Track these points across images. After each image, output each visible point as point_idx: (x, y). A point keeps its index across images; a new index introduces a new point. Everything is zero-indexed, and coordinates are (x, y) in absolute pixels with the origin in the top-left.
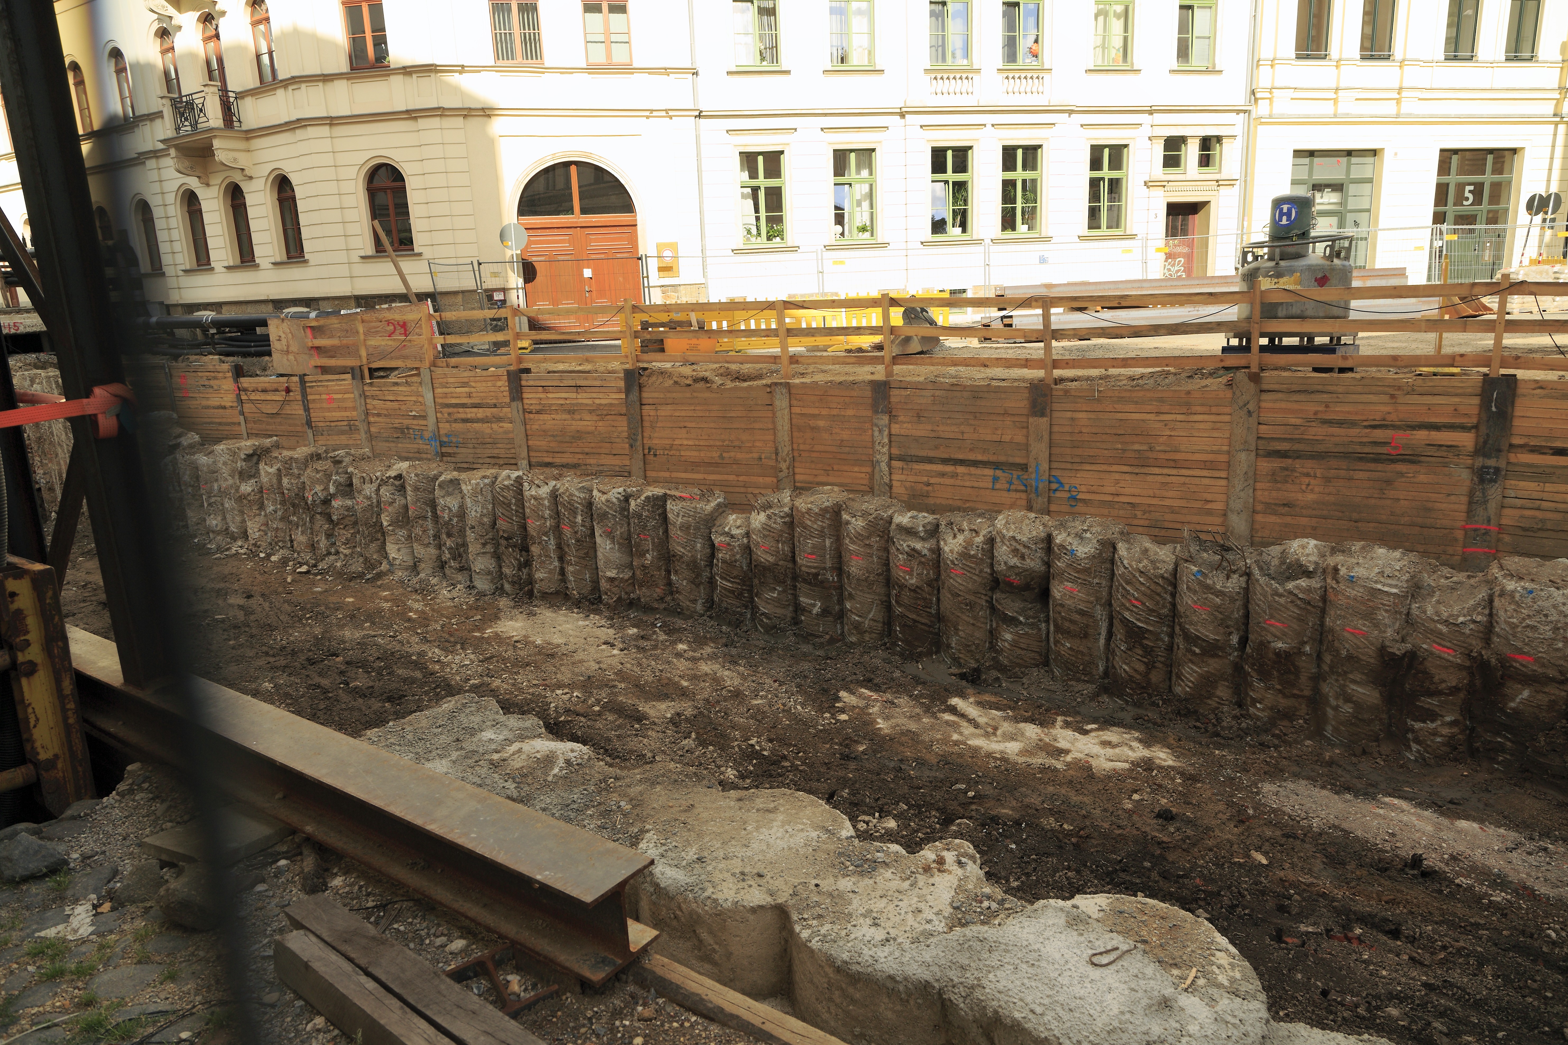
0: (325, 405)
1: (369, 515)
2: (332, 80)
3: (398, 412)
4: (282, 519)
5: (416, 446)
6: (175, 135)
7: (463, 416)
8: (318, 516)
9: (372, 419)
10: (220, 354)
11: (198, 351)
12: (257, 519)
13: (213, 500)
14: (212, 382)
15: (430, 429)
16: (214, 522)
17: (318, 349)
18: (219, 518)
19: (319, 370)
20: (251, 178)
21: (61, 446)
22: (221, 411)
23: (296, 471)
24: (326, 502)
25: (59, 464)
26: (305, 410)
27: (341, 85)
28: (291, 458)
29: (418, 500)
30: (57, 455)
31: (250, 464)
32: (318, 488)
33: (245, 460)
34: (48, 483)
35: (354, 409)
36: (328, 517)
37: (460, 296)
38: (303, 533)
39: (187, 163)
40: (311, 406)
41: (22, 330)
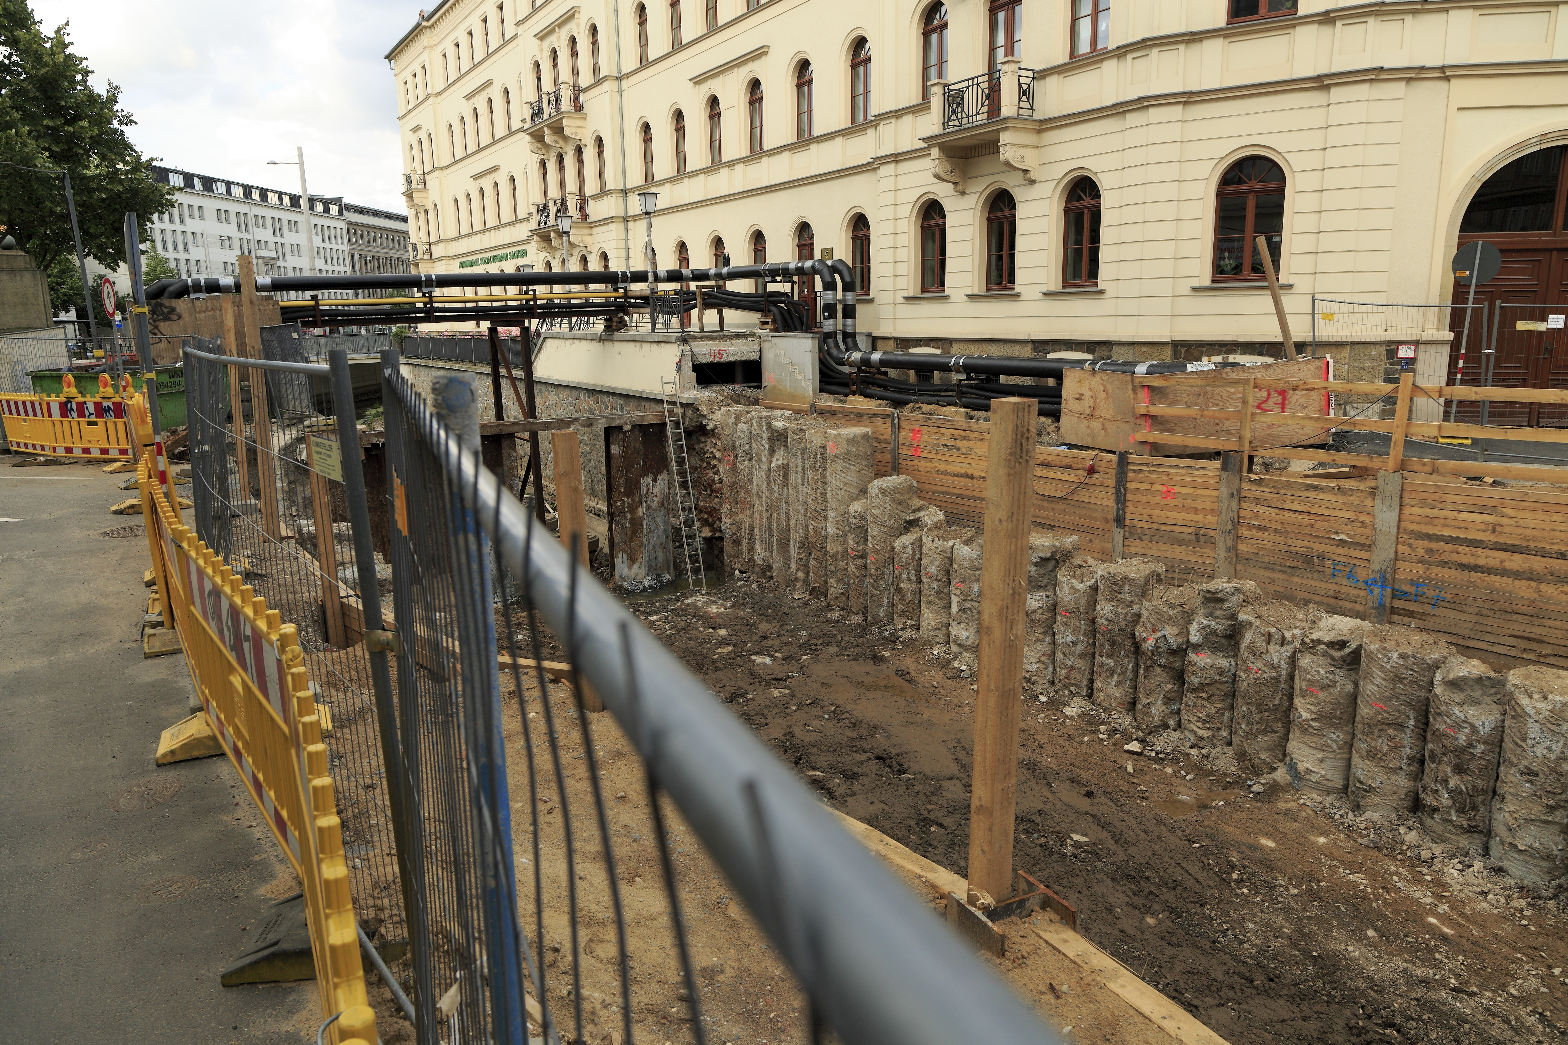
0: (1156, 499)
1: (1268, 692)
2: (1201, 40)
3: (1306, 530)
4: (1082, 655)
5: (1331, 586)
6: (941, 131)
7: (1465, 559)
8: (1158, 670)
9: (1245, 532)
10: (965, 407)
11: (935, 399)
12: (1038, 646)
13: (969, 605)
14: (959, 443)
15: (1375, 566)
16: (965, 634)
17: (1152, 418)
18: (972, 630)
19: (1147, 448)
20: (1033, 182)
21: (759, 497)
22: (965, 480)
23: (1128, 597)
24: (1180, 652)
25: (752, 515)
26: (1118, 501)
27: (1214, 46)
28: (1125, 578)
29: (1393, 696)
30: (752, 506)
31: (1042, 571)
32: (1170, 631)
33: (1036, 564)
34: (733, 534)
35: (1212, 512)
36: (1180, 677)
37: (1348, 347)
38: (1118, 684)
39: (948, 166)
40: (1129, 497)
41: (725, 358)
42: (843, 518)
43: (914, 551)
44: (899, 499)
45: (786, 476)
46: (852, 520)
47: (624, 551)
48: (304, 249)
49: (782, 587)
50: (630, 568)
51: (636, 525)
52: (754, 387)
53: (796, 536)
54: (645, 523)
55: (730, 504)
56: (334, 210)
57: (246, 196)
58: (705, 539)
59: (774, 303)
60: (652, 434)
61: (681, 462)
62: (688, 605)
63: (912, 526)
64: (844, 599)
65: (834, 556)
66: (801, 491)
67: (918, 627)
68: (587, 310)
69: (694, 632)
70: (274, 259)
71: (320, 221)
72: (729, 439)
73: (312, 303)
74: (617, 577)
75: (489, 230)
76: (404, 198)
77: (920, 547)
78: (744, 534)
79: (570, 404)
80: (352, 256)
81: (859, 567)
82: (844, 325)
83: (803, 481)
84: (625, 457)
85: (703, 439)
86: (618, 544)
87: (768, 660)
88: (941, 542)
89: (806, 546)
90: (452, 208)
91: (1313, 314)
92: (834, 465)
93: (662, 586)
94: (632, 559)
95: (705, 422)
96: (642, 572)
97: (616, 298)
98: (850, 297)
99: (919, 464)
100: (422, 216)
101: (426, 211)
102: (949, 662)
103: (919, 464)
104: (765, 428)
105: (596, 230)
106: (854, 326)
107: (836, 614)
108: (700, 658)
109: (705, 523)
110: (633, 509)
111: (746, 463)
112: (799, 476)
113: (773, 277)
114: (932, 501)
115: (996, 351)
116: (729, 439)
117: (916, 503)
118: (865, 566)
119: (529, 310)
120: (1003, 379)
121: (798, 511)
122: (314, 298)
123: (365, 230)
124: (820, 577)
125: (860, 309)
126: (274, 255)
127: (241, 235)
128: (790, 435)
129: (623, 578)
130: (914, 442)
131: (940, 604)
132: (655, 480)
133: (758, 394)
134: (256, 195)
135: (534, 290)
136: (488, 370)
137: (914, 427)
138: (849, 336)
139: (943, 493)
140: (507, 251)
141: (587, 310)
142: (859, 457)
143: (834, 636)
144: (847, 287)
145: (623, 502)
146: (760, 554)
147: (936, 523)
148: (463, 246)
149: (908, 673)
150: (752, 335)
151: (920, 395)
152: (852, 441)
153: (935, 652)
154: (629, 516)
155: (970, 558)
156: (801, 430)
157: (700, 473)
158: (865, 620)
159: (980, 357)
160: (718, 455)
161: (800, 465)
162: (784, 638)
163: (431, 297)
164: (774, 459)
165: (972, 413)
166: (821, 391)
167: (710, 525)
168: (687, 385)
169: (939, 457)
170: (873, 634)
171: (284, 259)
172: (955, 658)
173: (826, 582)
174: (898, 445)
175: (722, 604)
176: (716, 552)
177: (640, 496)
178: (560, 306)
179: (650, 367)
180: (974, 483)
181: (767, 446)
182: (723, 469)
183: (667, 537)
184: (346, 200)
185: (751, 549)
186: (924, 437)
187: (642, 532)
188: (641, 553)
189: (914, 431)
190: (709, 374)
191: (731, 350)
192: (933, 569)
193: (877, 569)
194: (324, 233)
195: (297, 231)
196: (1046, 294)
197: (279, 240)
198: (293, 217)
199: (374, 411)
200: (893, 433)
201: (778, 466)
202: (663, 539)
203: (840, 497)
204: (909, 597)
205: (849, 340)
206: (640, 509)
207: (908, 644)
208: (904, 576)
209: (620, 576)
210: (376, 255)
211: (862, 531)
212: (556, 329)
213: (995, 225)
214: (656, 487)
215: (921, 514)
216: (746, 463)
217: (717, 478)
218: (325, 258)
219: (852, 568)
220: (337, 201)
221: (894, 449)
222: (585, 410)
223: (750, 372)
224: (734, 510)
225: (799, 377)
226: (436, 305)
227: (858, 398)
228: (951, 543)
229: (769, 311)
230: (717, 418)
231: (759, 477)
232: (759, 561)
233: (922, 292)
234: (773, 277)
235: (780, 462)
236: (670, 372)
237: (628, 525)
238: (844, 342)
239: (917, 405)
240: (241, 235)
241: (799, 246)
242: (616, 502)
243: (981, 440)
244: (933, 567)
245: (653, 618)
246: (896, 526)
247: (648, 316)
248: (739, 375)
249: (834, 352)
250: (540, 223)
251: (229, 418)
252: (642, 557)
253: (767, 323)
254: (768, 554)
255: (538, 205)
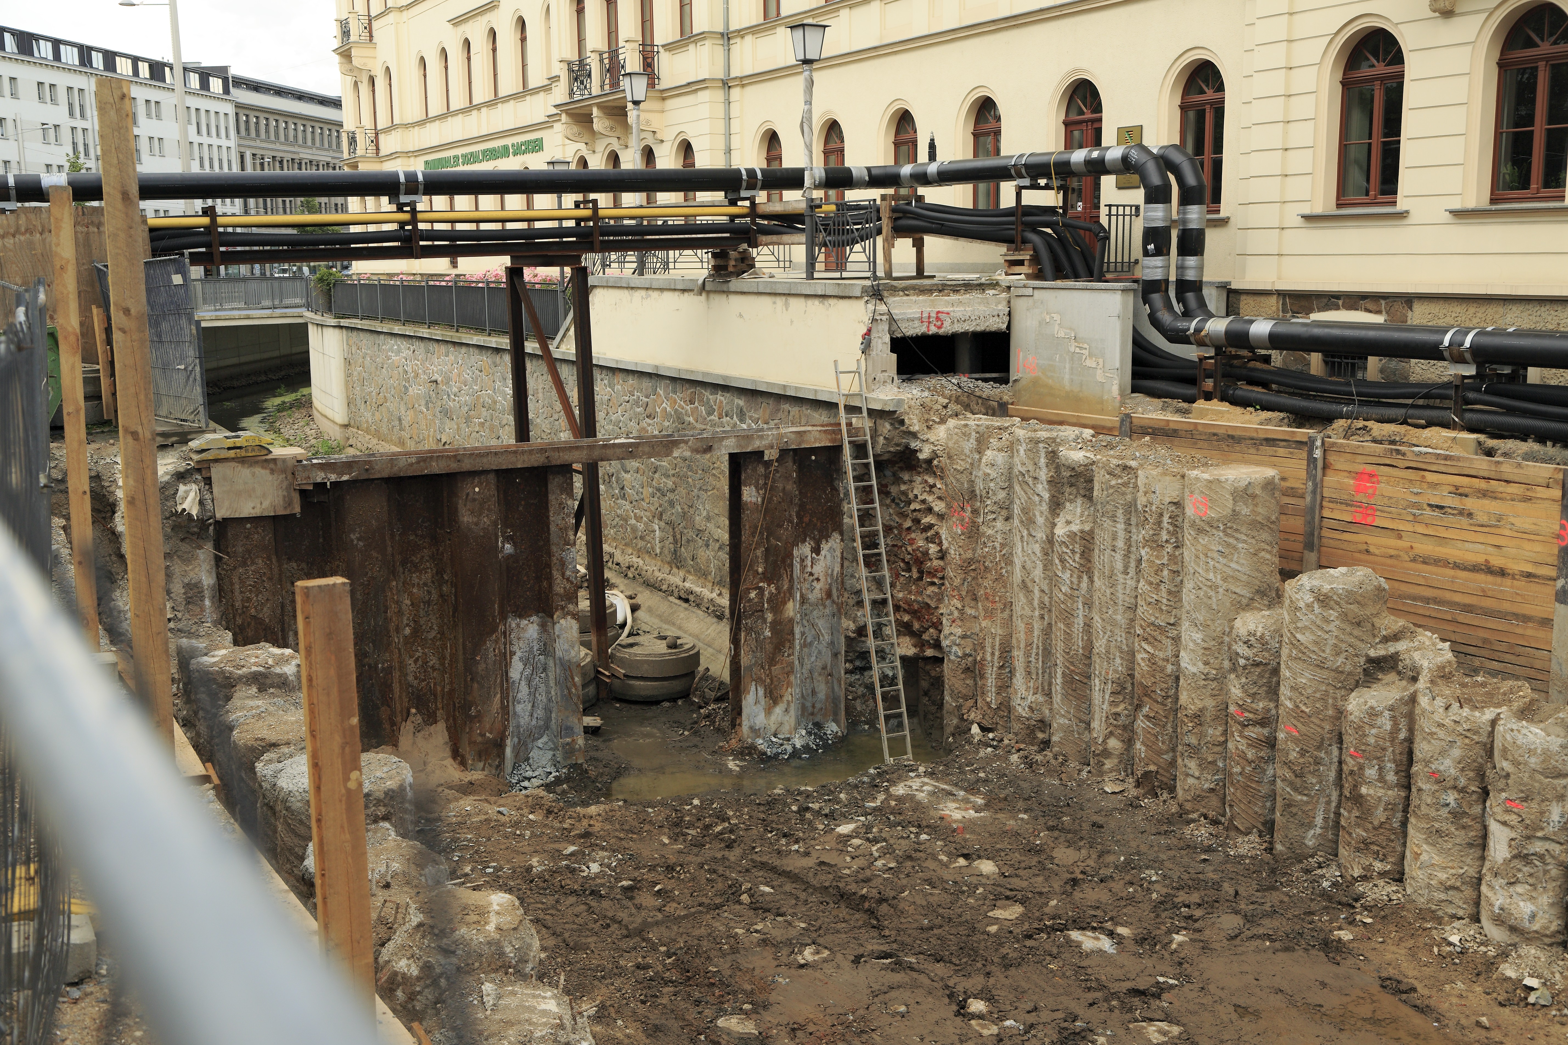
10: (1472, 430)
13: (1538, 847)
14: (1470, 503)
22: (1482, 579)
30: (1008, 605)
41: (948, 328)
42: (1220, 644)
43: (1395, 724)
44: (1356, 613)
45: (1087, 554)
46: (1241, 649)
47: (759, 681)
48: (170, 146)
49: (1073, 764)
50: (768, 711)
51: (783, 635)
52: (995, 380)
53: (1106, 671)
54: (797, 630)
55: (961, 598)
56: (216, 85)
57: (82, 63)
58: (903, 659)
59: (1033, 227)
60: (815, 466)
61: (866, 517)
62: (900, 799)
63: (1382, 669)
64: (1214, 802)
65: (1198, 717)
66: (1119, 584)
67: (1399, 878)
68: (685, 237)
69: (930, 864)
71: (194, 102)
72: (964, 478)
73: (206, 220)
74: (745, 728)
75: (478, 107)
76: (336, 58)
77: (1411, 718)
78: (991, 657)
79: (637, 403)
80: (242, 157)
81: (1254, 743)
82: (1181, 268)
83: (1126, 567)
84: (767, 508)
85: (906, 476)
86: (749, 668)
87: (1106, 944)
88: (1466, 711)
89: (1130, 691)
90: (415, 72)
92: (1204, 540)
93: (826, 746)
94: (773, 697)
95: (914, 445)
96: (790, 720)
97: (733, 217)
98: (1195, 214)
99: (1370, 540)
100: (364, 88)
101: (372, 80)
102: (1491, 965)
103: (1370, 540)
104: (1043, 461)
105: (671, 104)
106: (1200, 268)
107: (1201, 832)
108: (963, 930)
109: (905, 629)
110: (777, 604)
111: (999, 524)
112: (1118, 557)
113: (1034, 177)
114: (1423, 622)
115: (1514, 321)
116: (964, 478)
117: (1390, 623)
118: (1271, 743)
119: (598, 237)
120: (1534, 375)
121: (1114, 623)
122: (209, 212)
123: (262, 116)
124: (1159, 753)
125: (1212, 238)
128: (1100, 477)
129: (755, 731)
130: (1360, 497)
131: (1461, 837)
132: (817, 550)
133: (1003, 392)
135: (595, 202)
136: (504, 342)
137: (1360, 468)
138: (1189, 288)
139: (1427, 600)
140: (509, 141)
141: (685, 237)
142: (1255, 525)
143: (1217, 886)
144: (1187, 199)
145: (761, 590)
146: (1024, 697)
147: (1441, 668)
148: (433, 135)
149: (1414, 989)
150: (994, 285)
151: (1362, 403)
152: (1244, 494)
153: (1455, 939)
154: (769, 617)
155: (1546, 752)
156: (1125, 468)
157: (899, 537)
158: (1270, 850)
159: (1518, 334)
160: (939, 506)
161: (1121, 534)
162: (1117, 886)
163: (414, 212)
164: (1060, 521)
165: (1491, 443)
166: (1134, 390)
167: (916, 635)
168: (880, 376)
169: (1421, 529)
170: (1295, 885)
172: (1504, 955)
173: (1173, 763)
174: (1319, 499)
175: (966, 801)
176: (924, 684)
177: (791, 580)
178: (628, 231)
179: (808, 341)
180: (1506, 586)
181: (1046, 496)
182: (949, 533)
183: (836, 655)
184: (236, 71)
185: (1005, 686)
186: (1384, 488)
187: (792, 647)
188: (789, 684)
189: (1359, 476)
190: (920, 355)
191: (959, 311)
192: (1448, 766)
193: (1303, 753)
194: (200, 121)
195: (159, 117)
196: (1308, 218)
198: (154, 95)
199: (277, 401)
200: (1311, 476)
201: (1072, 535)
202: (827, 658)
203: (1214, 603)
204: (1380, 815)
205: (1190, 296)
206: (790, 605)
207: (1387, 913)
208: (1371, 773)
209: (751, 728)
210: (279, 155)
211: (1267, 674)
212: (613, 271)
213: (1191, 114)
214: (820, 563)
215: (1401, 646)
216: (999, 524)
217: (933, 549)
218: (201, 159)
219: (1237, 743)
220: (221, 72)
221: (1311, 510)
222: (666, 415)
223: (990, 353)
224: (969, 611)
225: (1091, 363)
226: (421, 226)
227: (1216, 406)
228: (1489, 714)
229: (1024, 241)
230: (938, 437)
231: (1026, 554)
232: (1021, 710)
233: (1339, 206)
234: (1034, 177)
235: (1075, 528)
236: (850, 353)
237: (768, 633)
238: (1180, 299)
239: (1360, 423)
241: (1066, 124)
242: (748, 591)
243: (1527, 499)
244: (1448, 762)
245: (845, 829)
246: (1348, 668)
247: (803, 249)
248: (964, 356)
249: (1166, 318)
250: (571, 93)
251: (57, 430)
252: (791, 694)
253: (1020, 263)
254: (1040, 698)
255: (569, 63)
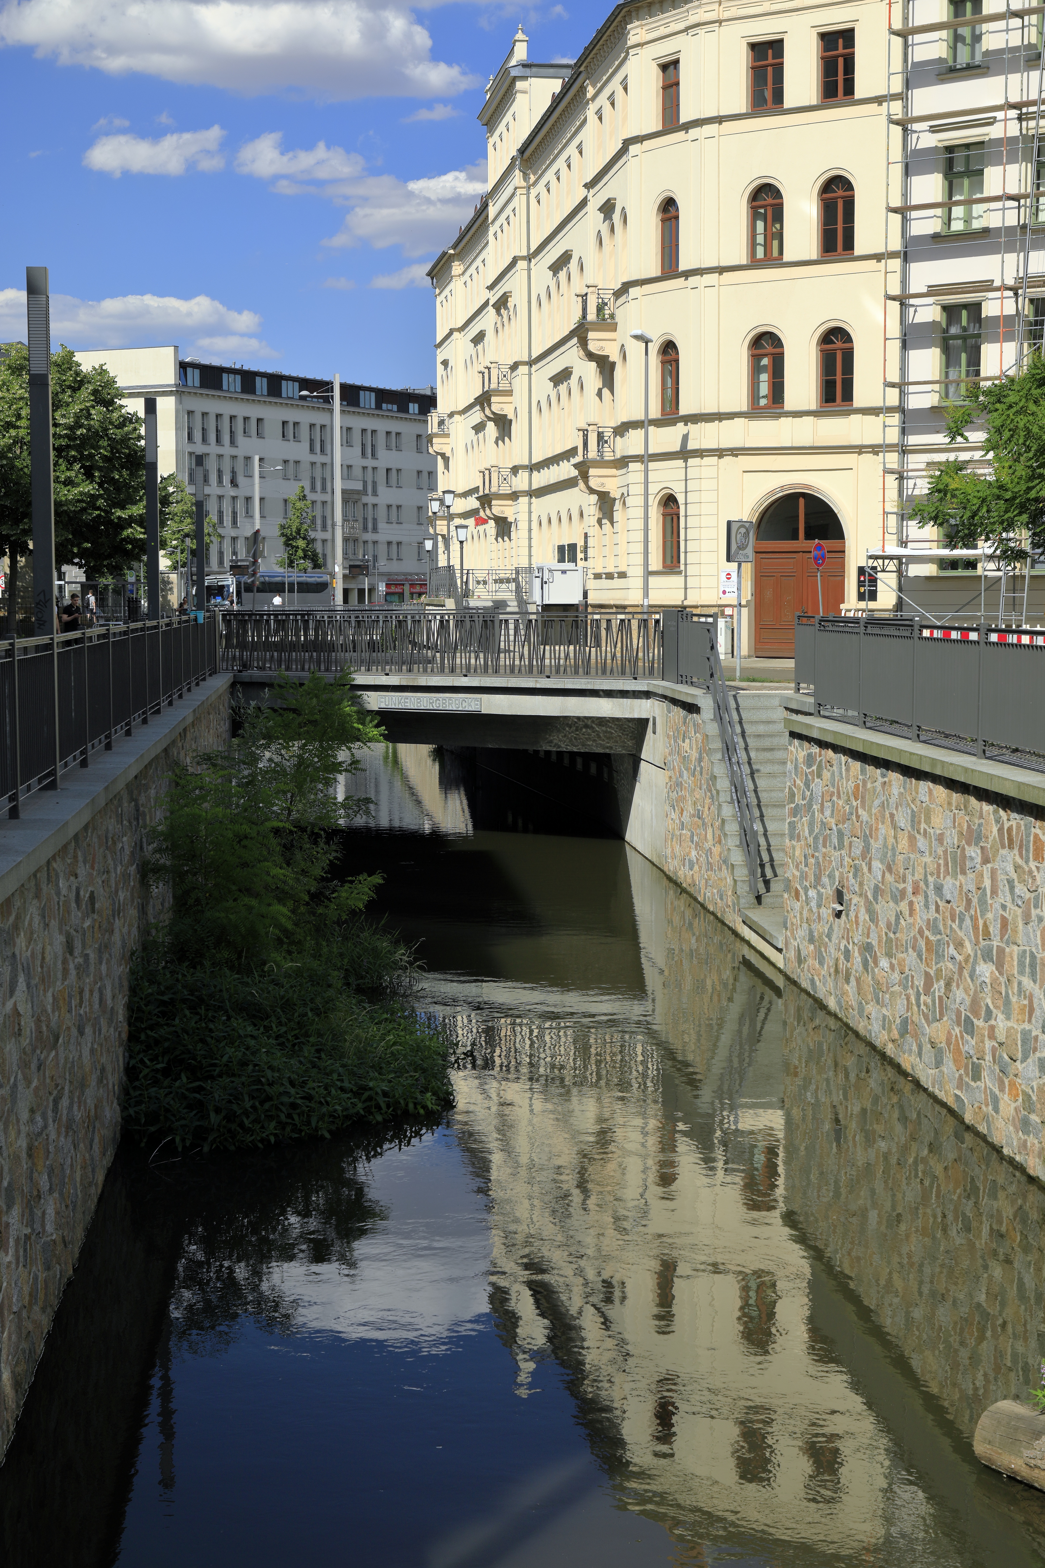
70: (358, 492)
91: (686, 589)
126: (359, 486)
127: (313, 458)
134: (261, 385)
171: (375, 493)
197: (370, 463)
240: (313, 458)
